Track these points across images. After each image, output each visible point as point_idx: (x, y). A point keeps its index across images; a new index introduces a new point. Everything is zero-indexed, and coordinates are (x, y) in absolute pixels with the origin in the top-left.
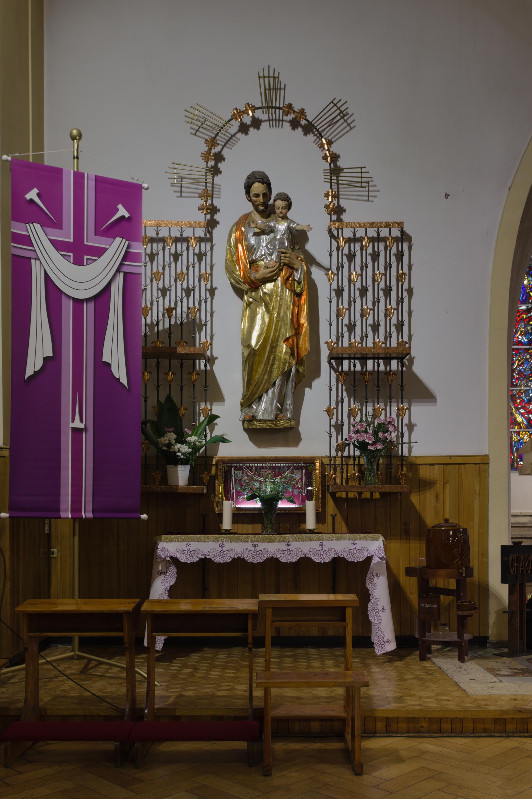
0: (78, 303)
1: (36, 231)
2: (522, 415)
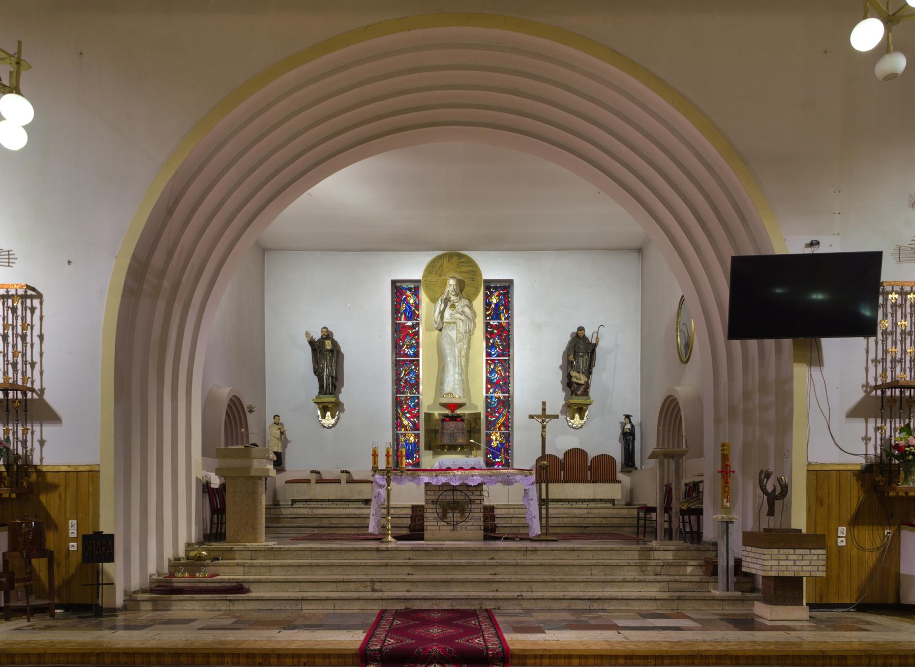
2: (408, 419)
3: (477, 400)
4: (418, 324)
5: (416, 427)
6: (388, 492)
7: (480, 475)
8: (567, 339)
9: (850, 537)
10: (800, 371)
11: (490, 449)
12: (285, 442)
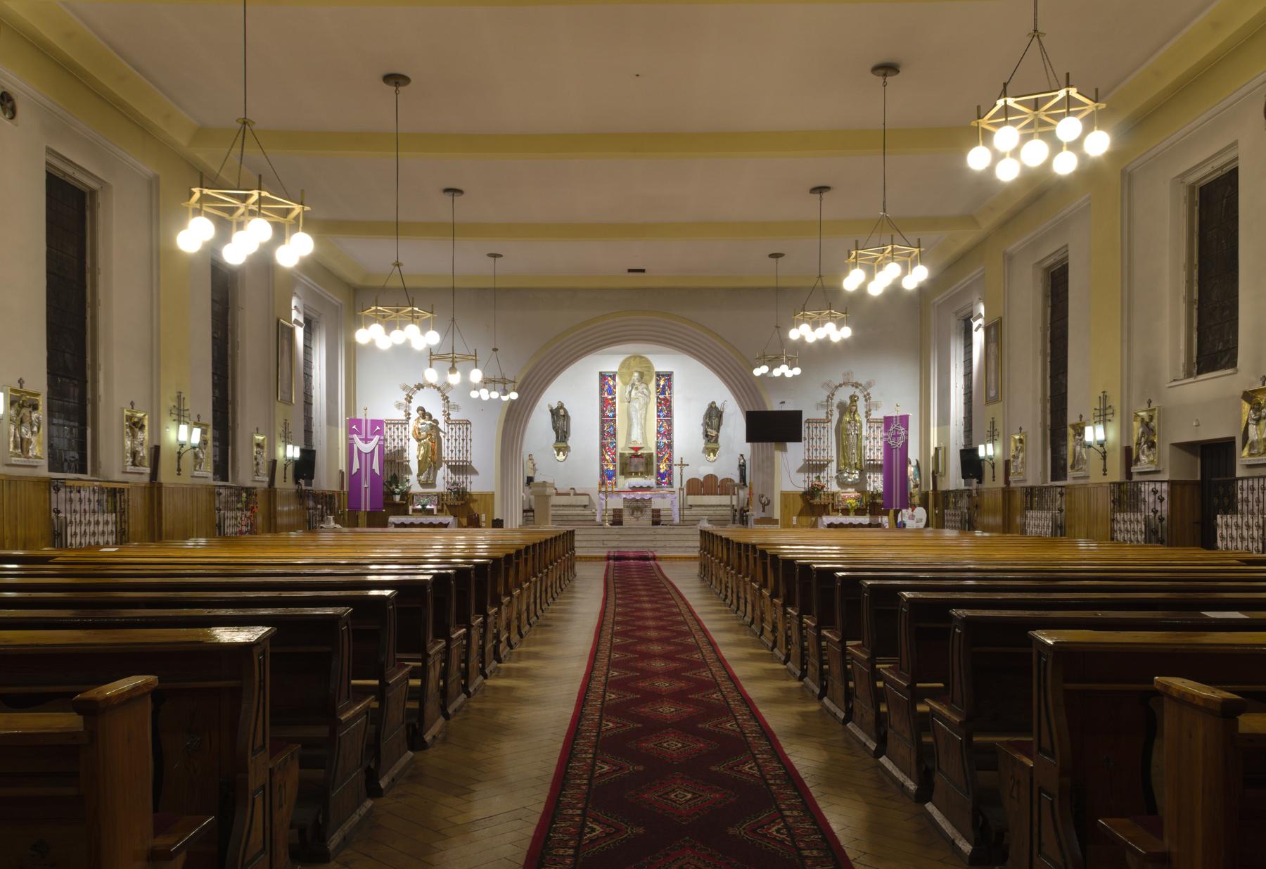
1: (355, 437)
5: (614, 461)
8: (707, 407)
10: (778, 454)
11: (659, 474)
12: (535, 470)
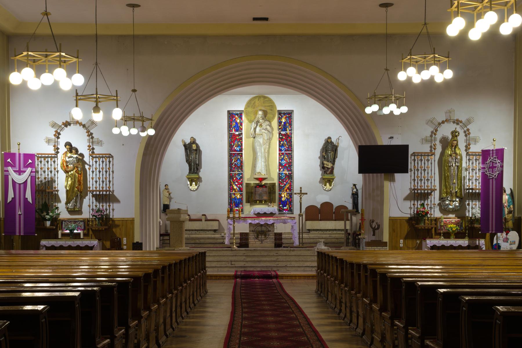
0: (20, 184)
1: (10, 169)
2: (237, 185)
3: (274, 178)
4: (242, 134)
5: (241, 190)
6: (234, 227)
7: (273, 220)
8: (323, 142)
9: (404, 243)
12: (170, 199)
